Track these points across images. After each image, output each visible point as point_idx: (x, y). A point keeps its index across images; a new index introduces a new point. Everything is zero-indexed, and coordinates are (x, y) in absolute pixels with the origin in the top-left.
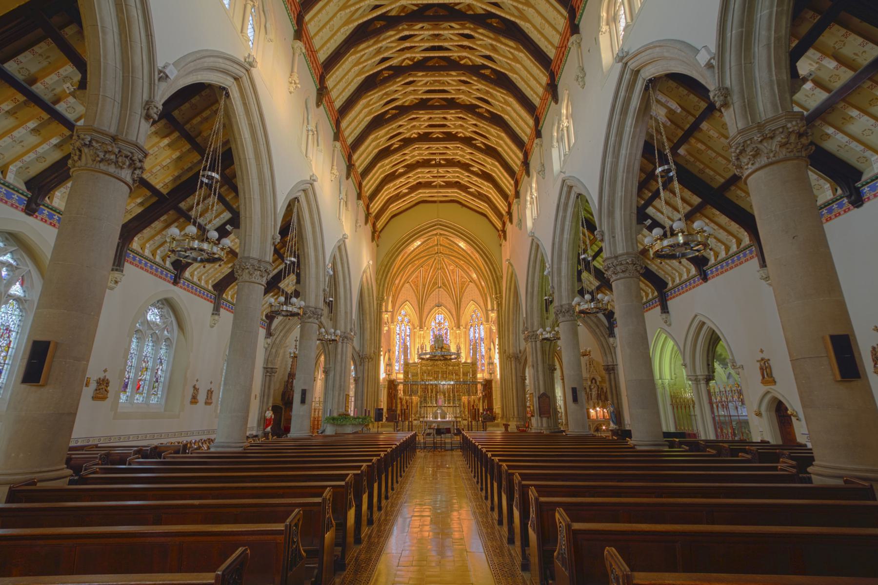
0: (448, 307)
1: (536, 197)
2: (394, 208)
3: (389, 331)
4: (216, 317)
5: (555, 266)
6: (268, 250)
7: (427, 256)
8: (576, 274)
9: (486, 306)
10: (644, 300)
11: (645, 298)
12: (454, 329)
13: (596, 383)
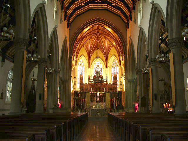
0: (102, 58)
1: (142, 10)
2: (78, 12)
3: (75, 69)
4: (3, 63)
5: (149, 41)
6: (27, 34)
7: (92, 34)
8: (158, 45)
9: (120, 58)
10: (184, 58)
11: (184, 57)
12: (105, 68)
13: (166, 92)
